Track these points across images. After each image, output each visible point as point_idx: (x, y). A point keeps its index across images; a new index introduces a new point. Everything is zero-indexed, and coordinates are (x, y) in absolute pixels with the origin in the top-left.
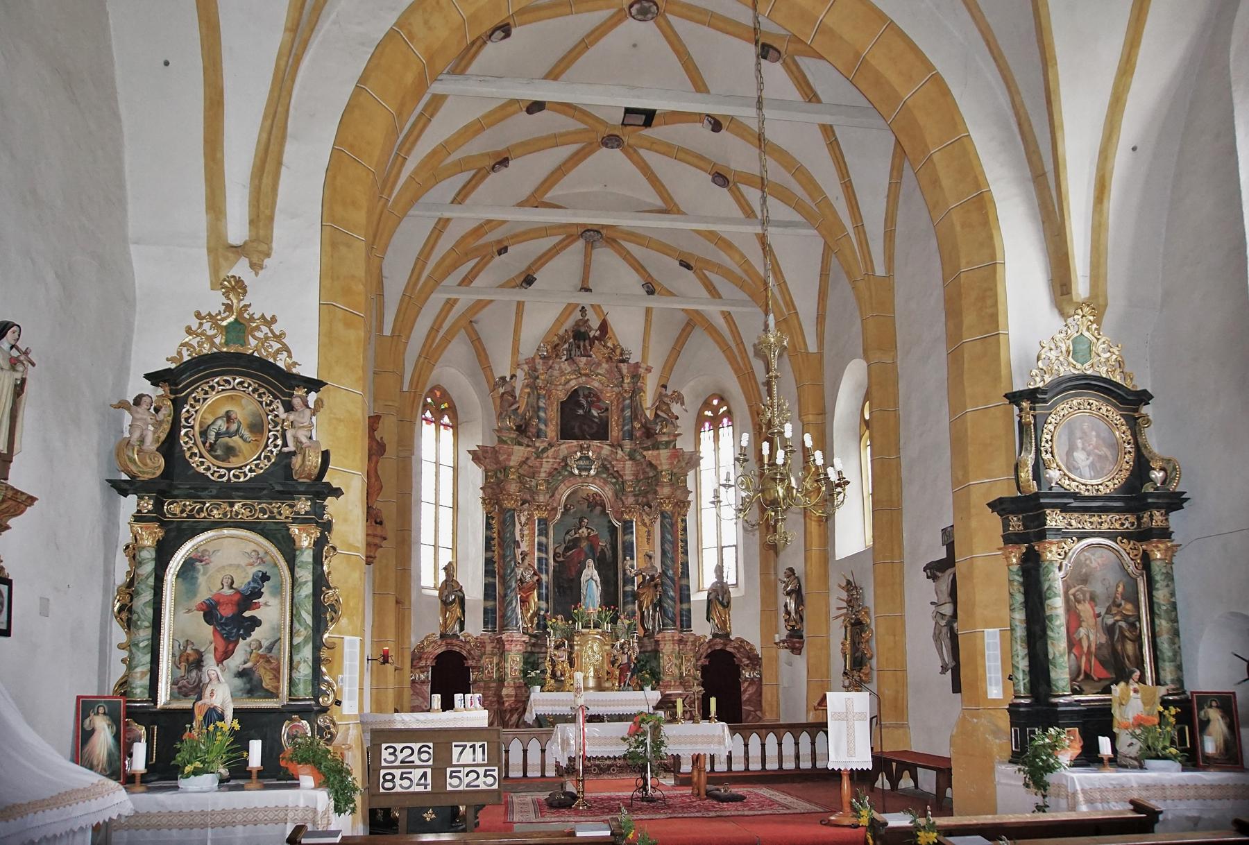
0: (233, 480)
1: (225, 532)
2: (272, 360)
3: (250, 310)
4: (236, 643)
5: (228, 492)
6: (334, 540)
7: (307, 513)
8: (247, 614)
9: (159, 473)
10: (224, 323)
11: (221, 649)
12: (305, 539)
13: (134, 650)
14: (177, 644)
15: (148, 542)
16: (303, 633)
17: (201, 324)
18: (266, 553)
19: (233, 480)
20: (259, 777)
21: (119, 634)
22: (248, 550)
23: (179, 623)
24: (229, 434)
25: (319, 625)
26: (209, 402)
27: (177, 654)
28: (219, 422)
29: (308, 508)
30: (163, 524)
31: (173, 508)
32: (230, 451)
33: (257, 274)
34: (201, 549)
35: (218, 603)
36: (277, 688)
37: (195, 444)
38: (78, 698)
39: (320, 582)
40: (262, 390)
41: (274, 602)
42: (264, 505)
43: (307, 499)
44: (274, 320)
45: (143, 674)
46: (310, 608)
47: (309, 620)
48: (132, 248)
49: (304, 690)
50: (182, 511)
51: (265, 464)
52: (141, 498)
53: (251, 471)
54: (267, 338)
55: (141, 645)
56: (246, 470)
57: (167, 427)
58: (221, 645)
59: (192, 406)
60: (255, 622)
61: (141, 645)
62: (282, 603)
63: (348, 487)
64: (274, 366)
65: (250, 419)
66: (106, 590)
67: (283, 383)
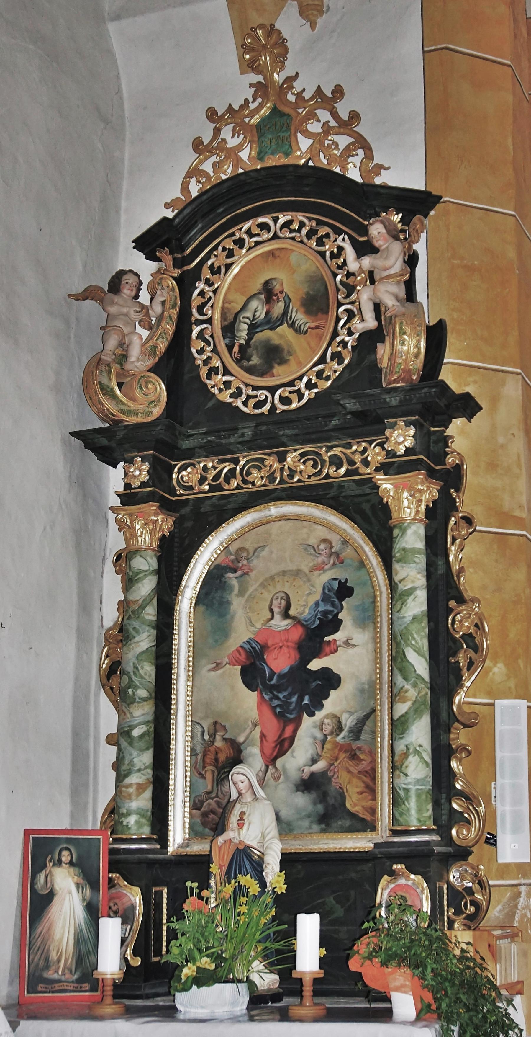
0: (281, 407)
1: (274, 510)
2: (338, 170)
3: (298, 86)
4: (298, 722)
5: (272, 433)
6: (467, 502)
7: (408, 451)
8: (315, 665)
9: (157, 411)
10: (255, 120)
11: (272, 737)
12: (408, 500)
13: (124, 744)
14: (198, 729)
15: (145, 539)
16: (414, 692)
17: (217, 131)
18: (345, 542)
19: (281, 407)
20: (316, 993)
21: (107, 718)
22: (313, 541)
23: (204, 690)
24: (271, 323)
25: (444, 680)
26: (235, 270)
27: (199, 749)
28: (254, 304)
29: (409, 444)
30: (167, 506)
31: (188, 476)
32: (274, 355)
33: (313, 26)
34: (233, 548)
35: (264, 648)
36: (373, 811)
37: (215, 351)
38: (27, 832)
39: (444, 590)
40: (323, 231)
41: (361, 637)
42: (337, 451)
43: (408, 424)
44: (338, 92)
45: (141, 788)
46: (424, 644)
47: (420, 665)
48: (112, 27)
49: (418, 813)
50: (202, 480)
51: (334, 369)
52: (130, 461)
53: (309, 386)
54: (327, 130)
55: (136, 733)
56: (302, 385)
57: (169, 328)
58: (272, 726)
59: (209, 283)
60: (330, 680)
61: (136, 733)
62: (376, 640)
63: (495, 400)
64: (343, 179)
65: (304, 289)
66: (82, 636)
67: (350, 204)
